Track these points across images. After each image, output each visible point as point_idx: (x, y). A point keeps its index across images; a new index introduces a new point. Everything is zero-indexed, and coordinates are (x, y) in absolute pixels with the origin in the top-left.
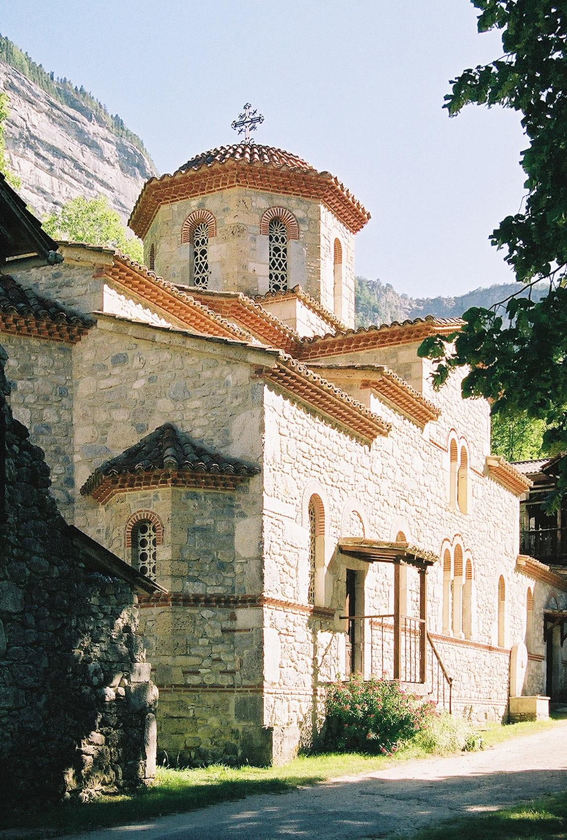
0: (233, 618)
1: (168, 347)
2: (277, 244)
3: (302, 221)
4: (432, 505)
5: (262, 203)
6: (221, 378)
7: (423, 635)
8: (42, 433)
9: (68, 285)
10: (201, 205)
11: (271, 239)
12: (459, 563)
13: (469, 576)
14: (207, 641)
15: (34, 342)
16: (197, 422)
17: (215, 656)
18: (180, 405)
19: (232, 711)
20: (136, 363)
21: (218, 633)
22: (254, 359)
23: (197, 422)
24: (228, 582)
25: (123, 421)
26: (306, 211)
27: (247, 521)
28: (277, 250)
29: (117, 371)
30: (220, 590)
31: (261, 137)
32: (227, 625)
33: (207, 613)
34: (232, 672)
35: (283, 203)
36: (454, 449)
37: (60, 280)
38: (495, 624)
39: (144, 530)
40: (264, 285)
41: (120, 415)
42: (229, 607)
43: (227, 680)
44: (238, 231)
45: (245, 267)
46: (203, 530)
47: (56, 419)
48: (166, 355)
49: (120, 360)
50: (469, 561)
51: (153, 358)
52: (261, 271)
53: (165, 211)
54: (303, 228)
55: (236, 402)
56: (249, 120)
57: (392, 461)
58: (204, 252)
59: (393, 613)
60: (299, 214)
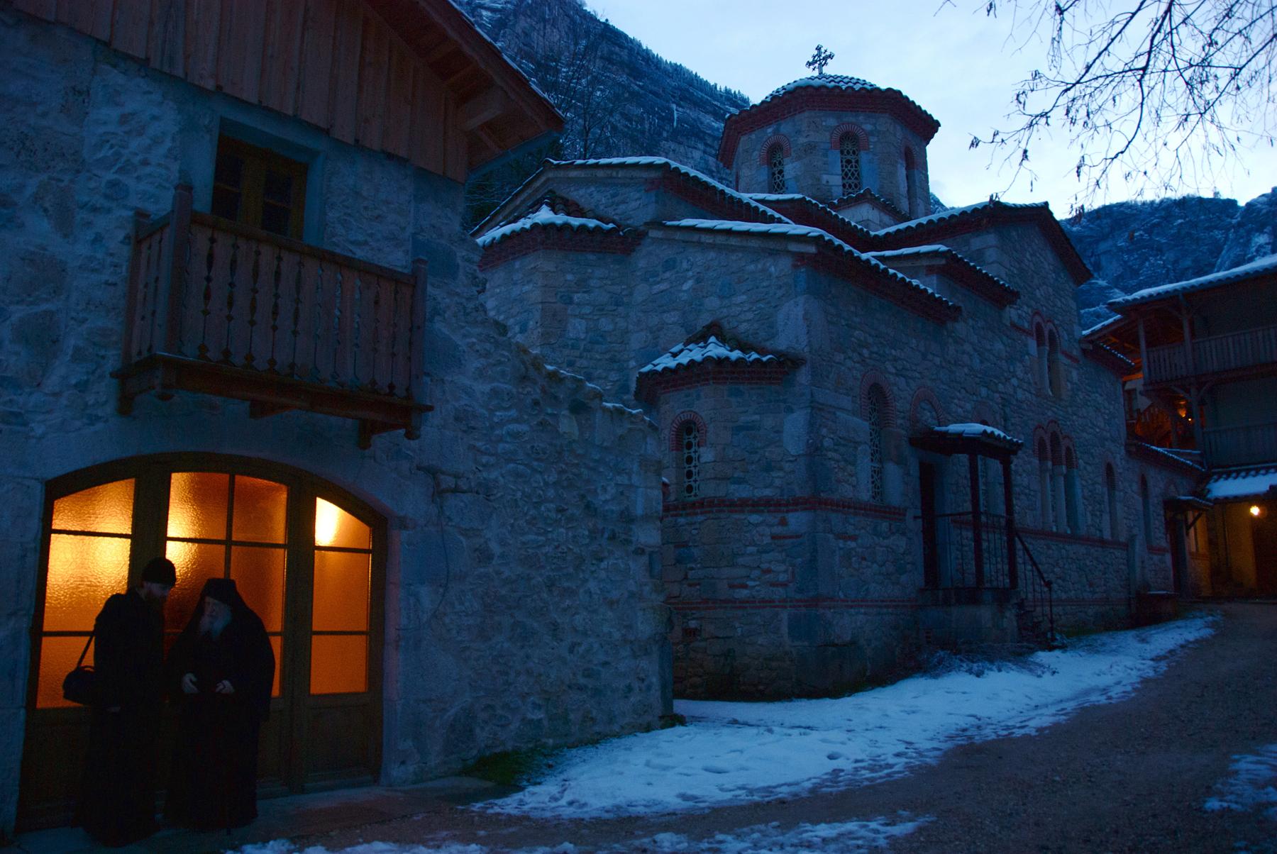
0: (783, 522)
1: (713, 246)
2: (849, 157)
3: (871, 133)
4: (1019, 391)
5: (832, 122)
6: (764, 270)
7: (1011, 531)
8: (598, 343)
9: (624, 202)
10: (776, 132)
11: (842, 152)
12: (1055, 449)
13: (1071, 464)
14: (755, 549)
15: (591, 257)
16: (743, 317)
17: (764, 566)
18: (726, 302)
19: (785, 630)
20: (685, 265)
21: (767, 540)
22: (793, 247)
23: (743, 317)
24: (778, 482)
25: (674, 323)
26: (874, 125)
27: (795, 415)
28: (849, 162)
29: (667, 275)
30: (768, 492)
31: (830, 69)
32: (778, 530)
33: (755, 518)
34: (784, 585)
35: (852, 120)
36: (1039, 329)
37: (616, 199)
38: (1106, 517)
39: (689, 431)
40: (837, 191)
41: (672, 318)
42: (779, 511)
43: (780, 593)
44: (810, 148)
45: (819, 180)
46: (747, 428)
47: (611, 327)
48: (712, 254)
49: (669, 265)
50: (1068, 449)
51: (699, 258)
52: (835, 180)
53: (744, 142)
54: (873, 139)
55: (779, 293)
56: (821, 58)
57: (968, 347)
58: (781, 172)
59: (46, 641)
60: (868, 127)
